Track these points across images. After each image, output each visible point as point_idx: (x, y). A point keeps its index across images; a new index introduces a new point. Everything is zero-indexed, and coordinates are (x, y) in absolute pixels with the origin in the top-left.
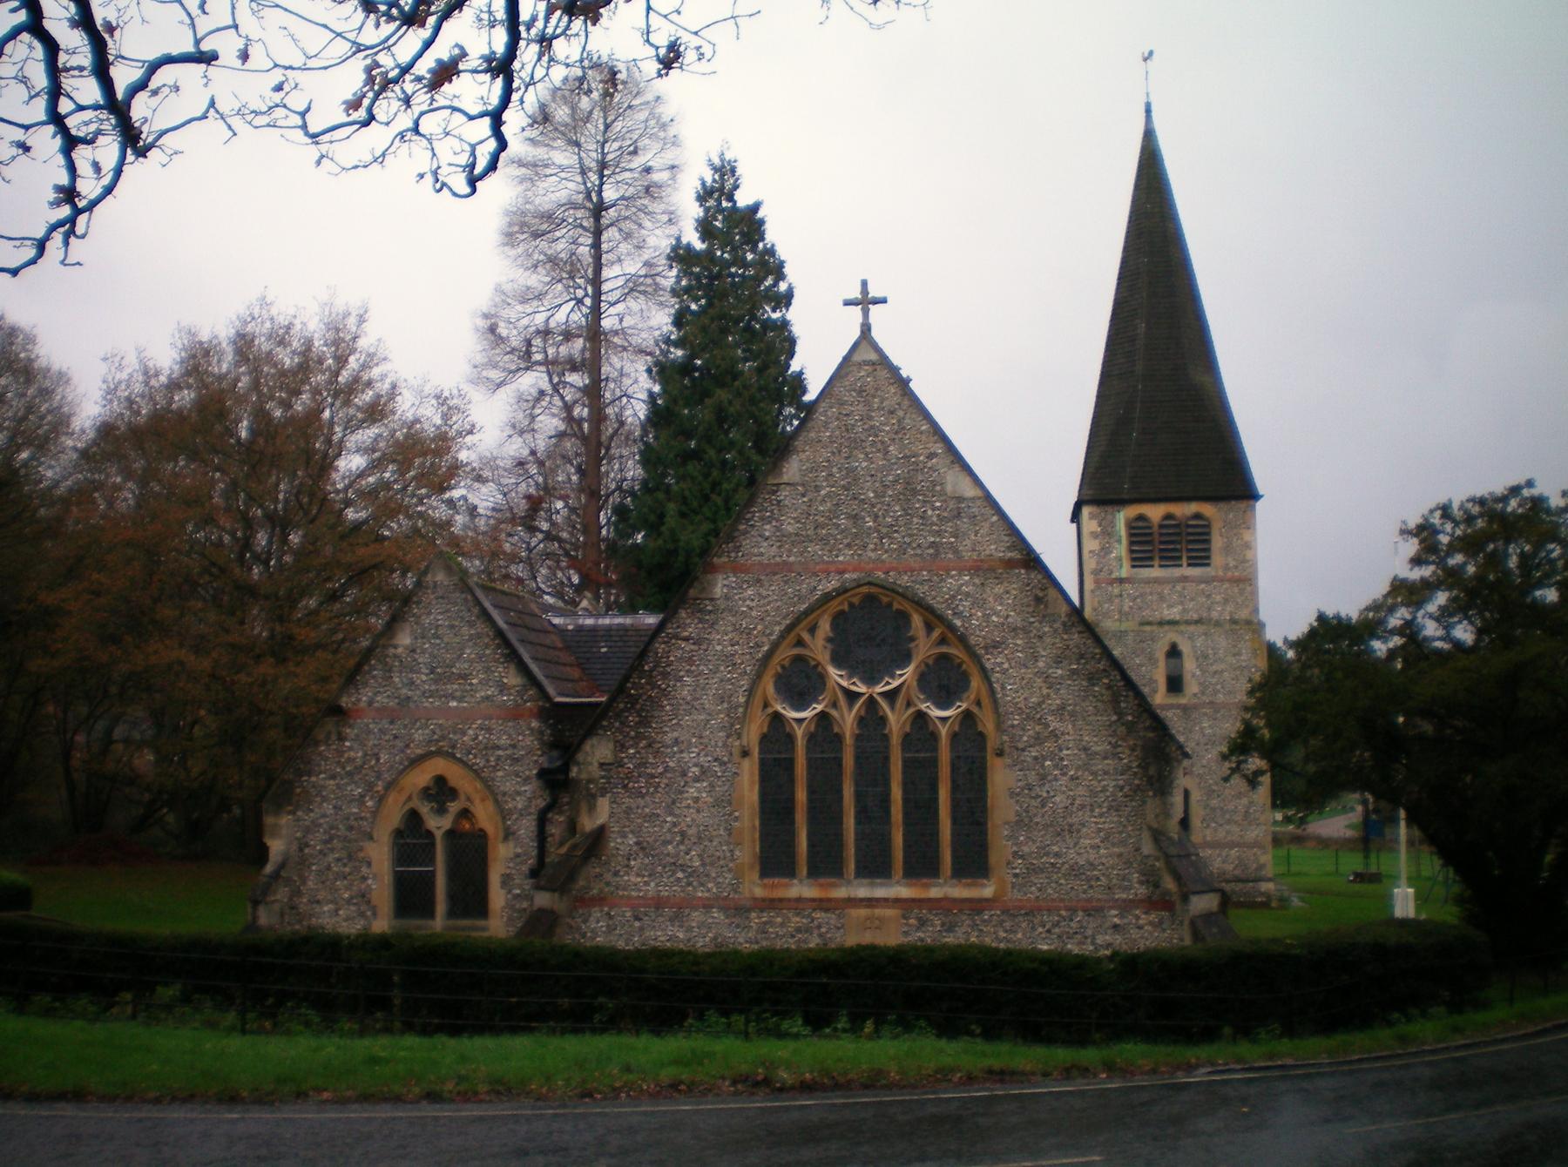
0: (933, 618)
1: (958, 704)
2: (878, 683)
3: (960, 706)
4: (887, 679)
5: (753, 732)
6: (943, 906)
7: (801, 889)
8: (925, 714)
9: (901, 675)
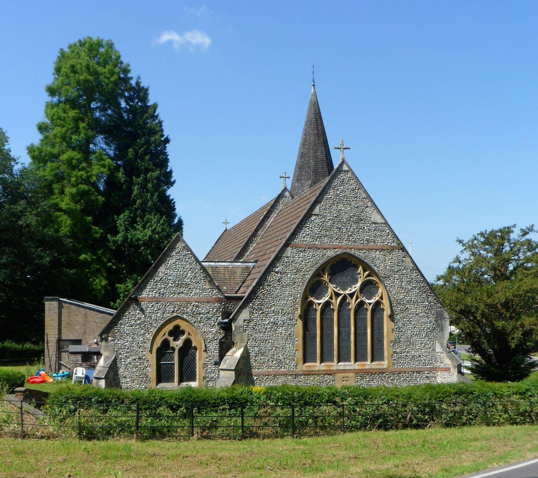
1: (375, 298)
5: (158, 343)
6: (370, 373)
7: (318, 366)
8: (364, 301)
9: (355, 287)
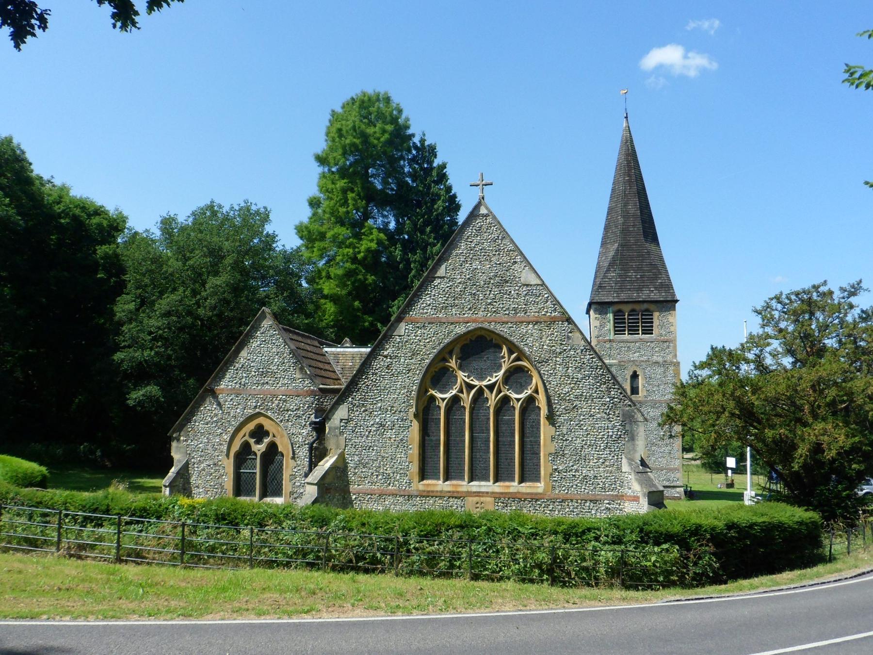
0: (513, 348)
2: (484, 380)
3: (527, 393)
4: (489, 378)
7: (440, 485)
9: (496, 376)
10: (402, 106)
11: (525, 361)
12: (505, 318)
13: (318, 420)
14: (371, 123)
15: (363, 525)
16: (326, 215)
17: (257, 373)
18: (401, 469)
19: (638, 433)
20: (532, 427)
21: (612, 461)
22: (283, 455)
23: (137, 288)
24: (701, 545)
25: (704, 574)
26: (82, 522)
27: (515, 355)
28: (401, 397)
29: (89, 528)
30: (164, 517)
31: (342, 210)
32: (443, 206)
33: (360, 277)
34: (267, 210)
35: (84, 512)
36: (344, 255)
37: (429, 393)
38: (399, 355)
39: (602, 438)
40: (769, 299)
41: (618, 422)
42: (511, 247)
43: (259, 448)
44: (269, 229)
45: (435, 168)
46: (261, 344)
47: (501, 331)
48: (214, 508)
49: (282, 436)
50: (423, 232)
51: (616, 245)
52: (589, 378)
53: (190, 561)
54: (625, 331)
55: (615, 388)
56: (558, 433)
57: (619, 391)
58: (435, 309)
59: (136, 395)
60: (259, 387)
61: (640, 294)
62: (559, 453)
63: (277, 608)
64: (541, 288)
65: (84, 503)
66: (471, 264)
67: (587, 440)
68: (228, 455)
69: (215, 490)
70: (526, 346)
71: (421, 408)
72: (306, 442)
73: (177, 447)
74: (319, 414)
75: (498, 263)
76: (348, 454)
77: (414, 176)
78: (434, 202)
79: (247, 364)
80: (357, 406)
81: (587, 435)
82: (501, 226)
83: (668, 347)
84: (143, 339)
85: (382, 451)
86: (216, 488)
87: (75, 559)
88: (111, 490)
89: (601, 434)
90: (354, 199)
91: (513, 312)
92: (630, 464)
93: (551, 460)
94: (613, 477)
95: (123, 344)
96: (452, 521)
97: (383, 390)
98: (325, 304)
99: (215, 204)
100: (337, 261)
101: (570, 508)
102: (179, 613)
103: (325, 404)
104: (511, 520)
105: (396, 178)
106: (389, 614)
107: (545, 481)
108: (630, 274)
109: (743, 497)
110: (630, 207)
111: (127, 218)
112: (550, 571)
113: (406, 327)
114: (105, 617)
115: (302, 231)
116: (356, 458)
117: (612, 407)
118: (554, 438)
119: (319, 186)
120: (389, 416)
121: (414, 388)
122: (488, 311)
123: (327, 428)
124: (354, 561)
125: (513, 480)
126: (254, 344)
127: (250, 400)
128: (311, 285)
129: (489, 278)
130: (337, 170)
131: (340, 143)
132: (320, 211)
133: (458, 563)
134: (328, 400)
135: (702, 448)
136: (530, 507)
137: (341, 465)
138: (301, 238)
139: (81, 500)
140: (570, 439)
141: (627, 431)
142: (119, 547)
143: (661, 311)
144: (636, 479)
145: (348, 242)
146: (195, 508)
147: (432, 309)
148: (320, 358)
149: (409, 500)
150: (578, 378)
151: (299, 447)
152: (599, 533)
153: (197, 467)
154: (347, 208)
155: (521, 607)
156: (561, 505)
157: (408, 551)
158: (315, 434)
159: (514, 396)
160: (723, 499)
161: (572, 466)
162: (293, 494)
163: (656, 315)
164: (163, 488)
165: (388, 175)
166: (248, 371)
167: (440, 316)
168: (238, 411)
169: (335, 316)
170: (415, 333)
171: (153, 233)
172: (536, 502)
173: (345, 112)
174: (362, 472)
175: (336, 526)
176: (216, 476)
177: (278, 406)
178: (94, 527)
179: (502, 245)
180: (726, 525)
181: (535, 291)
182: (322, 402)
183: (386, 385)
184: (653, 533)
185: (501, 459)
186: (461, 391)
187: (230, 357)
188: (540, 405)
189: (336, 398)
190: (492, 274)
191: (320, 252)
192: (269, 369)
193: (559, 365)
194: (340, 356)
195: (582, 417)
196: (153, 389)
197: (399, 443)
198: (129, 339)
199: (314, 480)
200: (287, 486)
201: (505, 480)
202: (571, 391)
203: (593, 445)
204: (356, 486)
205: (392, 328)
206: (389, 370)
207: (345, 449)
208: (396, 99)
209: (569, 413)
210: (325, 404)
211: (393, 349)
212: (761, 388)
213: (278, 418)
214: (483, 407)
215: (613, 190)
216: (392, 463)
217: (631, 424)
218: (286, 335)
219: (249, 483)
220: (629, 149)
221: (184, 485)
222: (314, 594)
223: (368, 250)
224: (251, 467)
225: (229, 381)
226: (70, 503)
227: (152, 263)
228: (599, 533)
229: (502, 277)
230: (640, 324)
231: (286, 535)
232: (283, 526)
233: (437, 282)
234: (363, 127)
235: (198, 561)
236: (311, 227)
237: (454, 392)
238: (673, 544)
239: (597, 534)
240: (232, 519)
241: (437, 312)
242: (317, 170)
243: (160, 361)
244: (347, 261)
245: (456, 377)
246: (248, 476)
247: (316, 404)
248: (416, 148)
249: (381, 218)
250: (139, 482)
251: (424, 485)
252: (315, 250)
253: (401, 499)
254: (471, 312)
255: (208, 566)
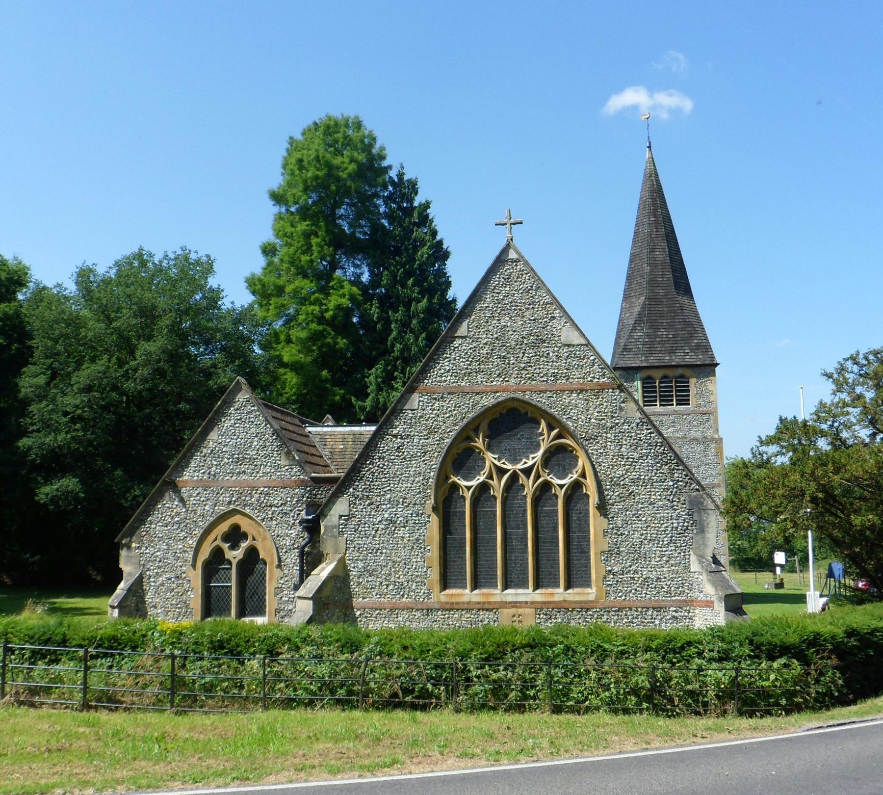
2: (519, 463)
4: (524, 460)
7: (466, 594)
9: (533, 458)
10: (376, 133)
11: (568, 439)
12: (543, 387)
13: (310, 517)
14: (338, 152)
15: (405, 648)
16: (284, 265)
17: (231, 460)
18: (417, 576)
19: (708, 524)
20: (579, 519)
21: (678, 558)
22: (265, 563)
23: (47, 357)
24: (822, 658)
25: (829, 693)
26: (30, 658)
27: (556, 431)
28: (416, 487)
29: (41, 665)
30: (141, 648)
31: (305, 258)
32: (427, 254)
33: (329, 340)
34: (210, 259)
35: (32, 644)
36: (308, 314)
37: (450, 481)
38: (412, 434)
39: (665, 531)
40: (844, 359)
41: (684, 511)
42: (548, 299)
43: (235, 555)
44: (213, 282)
45: (416, 207)
46: (235, 424)
47: (538, 401)
48: (208, 633)
49: (264, 539)
50: (404, 286)
51: (643, 298)
52: (647, 457)
53: (182, 704)
54: (656, 401)
55: (679, 470)
56: (611, 526)
57: (684, 473)
58: (456, 376)
59: (46, 492)
60: (234, 478)
61: (673, 357)
62: (613, 550)
63: (347, 764)
64: (586, 349)
65: (31, 633)
66: (499, 320)
67: (647, 533)
68: (194, 566)
69: (177, 610)
70: (570, 420)
71: (441, 500)
72: (296, 546)
73: (127, 557)
74: (311, 510)
75: (533, 318)
76: (349, 560)
77: (390, 216)
78: (415, 249)
79: (217, 449)
80: (361, 499)
81: (647, 527)
82: (535, 273)
83: (708, 420)
84: (57, 422)
85: (393, 555)
86: (179, 608)
87: (26, 707)
88: (25, 614)
89: (664, 525)
90: (318, 245)
91: (553, 379)
92: (701, 562)
93: (604, 560)
94: (680, 579)
95: (31, 428)
96: (518, 640)
97: (393, 478)
98: (285, 374)
99: (144, 252)
100: (300, 321)
101: (628, 618)
102: (234, 775)
103: (319, 496)
104: (591, 635)
105: (369, 220)
106: (493, 762)
107: (597, 587)
108: (660, 333)
109: (806, 598)
110: (658, 253)
111: (29, 269)
112: (649, 698)
113: (421, 399)
114: (139, 787)
115: (254, 284)
116: (360, 565)
117: (676, 492)
118: (607, 532)
119: (274, 230)
120: (401, 510)
121: (432, 474)
122: (521, 377)
123: (322, 527)
124: (401, 696)
125: (558, 586)
126: (227, 423)
127: (222, 494)
128: (267, 351)
129: (522, 338)
130: (297, 210)
131: (301, 177)
132: (276, 260)
133: (532, 693)
134: (322, 491)
135: (764, 540)
136: (579, 618)
137: (341, 574)
138: (253, 293)
139: (27, 629)
140: (626, 533)
141: (695, 521)
142: (85, 688)
143: (698, 377)
144: (709, 580)
145: (313, 297)
146: (181, 634)
147: (451, 376)
148: (304, 440)
149: (428, 615)
150: (633, 458)
151: (286, 552)
152: (701, 647)
153: (154, 582)
154: (311, 256)
155: (645, 746)
156: (618, 615)
157: (468, 679)
158: (306, 535)
159: (556, 481)
160: (776, 602)
161: (630, 566)
162: (279, 612)
163: (693, 381)
164: (109, 609)
165: (359, 216)
166: (219, 458)
167: (462, 384)
168: (207, 508)
169: (298, 388)
170: (432, 406)
171: (66, 289)
172: (586, 612)
173: (306, 139)
174: (368, 581)
175: (371, 651)
176: (179, 593)
177: (258, 501)
178: (48, 664)
179: (536, 297)
180: (846, 632)
181: (578, 352)
182: (316, 495)
183: (397, 471)
184: (765, 646)
185: (542, 560)
186: (490, 477)
187: (195, 440)
188: (588, 492)
189: (333, 489)
190: (525, 333)
191: (278, 310)
192: (247, 454)
193: (611, 442)
194: (327, 437)
195: (640, 506)
196: (70, 483)
197: (414, 544)
198: (39, 422)
199: (309, 592)
200: (271, 601)
201: (547, 586)
202: (626, 474)
203: (654, 540)
204: (361, 599)
205: (403, 401)
206: (399, 452)
207: (345, 554)
208: (369, 125)
209: (624, 500)
210: (319, 496)
211: (405, 427)
212: (845, 466)
213: (259, 516)
214: (518, 496)
215: (636, 233)
216: (406, 570)
217: (699, 513)
218: (265, 410)
219: (222, 600)
220: (653, 185)
221: (137, 605)
222: (379, 740)
223: (339, 307)
224: (225, 579)
225: (195, 471)
226: (12, 633)
227: (68, 325)
228: (701, 647)
229: (537, 336)
230: (674, 393)
231: (306, 666)
232: (302, 653)
233: (457, 343)
234: (328, 156)
235: (192, 703)
236: (266, 280)
237: (482, 478)
238: (791, 658)
239: (699, 649)
240: (233, 646)
241: (458, 380)
242: (272, 209)
243: (78, 448)
244: (312, 321)
245: (484, 460)
246: (221, 591)
247: (308, 498)
248: (391, 180)
249: (352, 269)
250: (55, 603)
251: (447, 595)
252: (271, 307)
253: (418, 614)
254: (501, 379)
255: (206, 709)
